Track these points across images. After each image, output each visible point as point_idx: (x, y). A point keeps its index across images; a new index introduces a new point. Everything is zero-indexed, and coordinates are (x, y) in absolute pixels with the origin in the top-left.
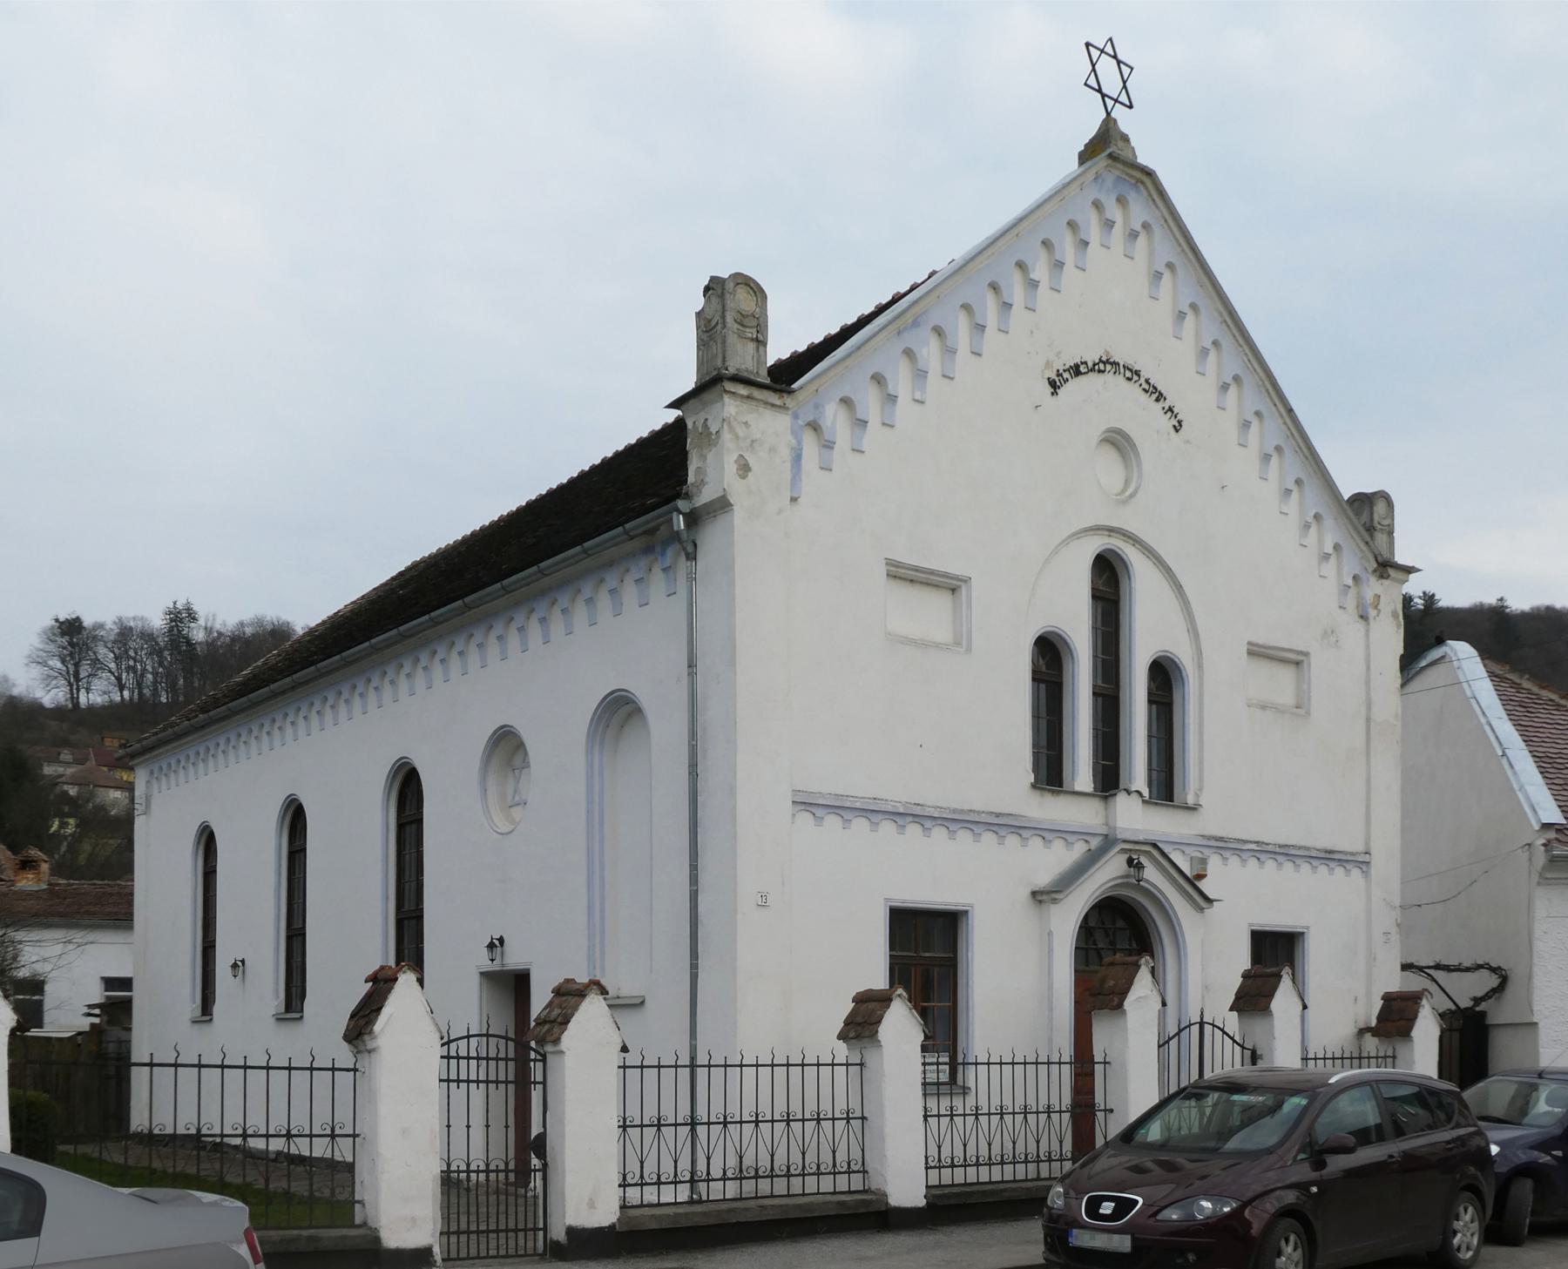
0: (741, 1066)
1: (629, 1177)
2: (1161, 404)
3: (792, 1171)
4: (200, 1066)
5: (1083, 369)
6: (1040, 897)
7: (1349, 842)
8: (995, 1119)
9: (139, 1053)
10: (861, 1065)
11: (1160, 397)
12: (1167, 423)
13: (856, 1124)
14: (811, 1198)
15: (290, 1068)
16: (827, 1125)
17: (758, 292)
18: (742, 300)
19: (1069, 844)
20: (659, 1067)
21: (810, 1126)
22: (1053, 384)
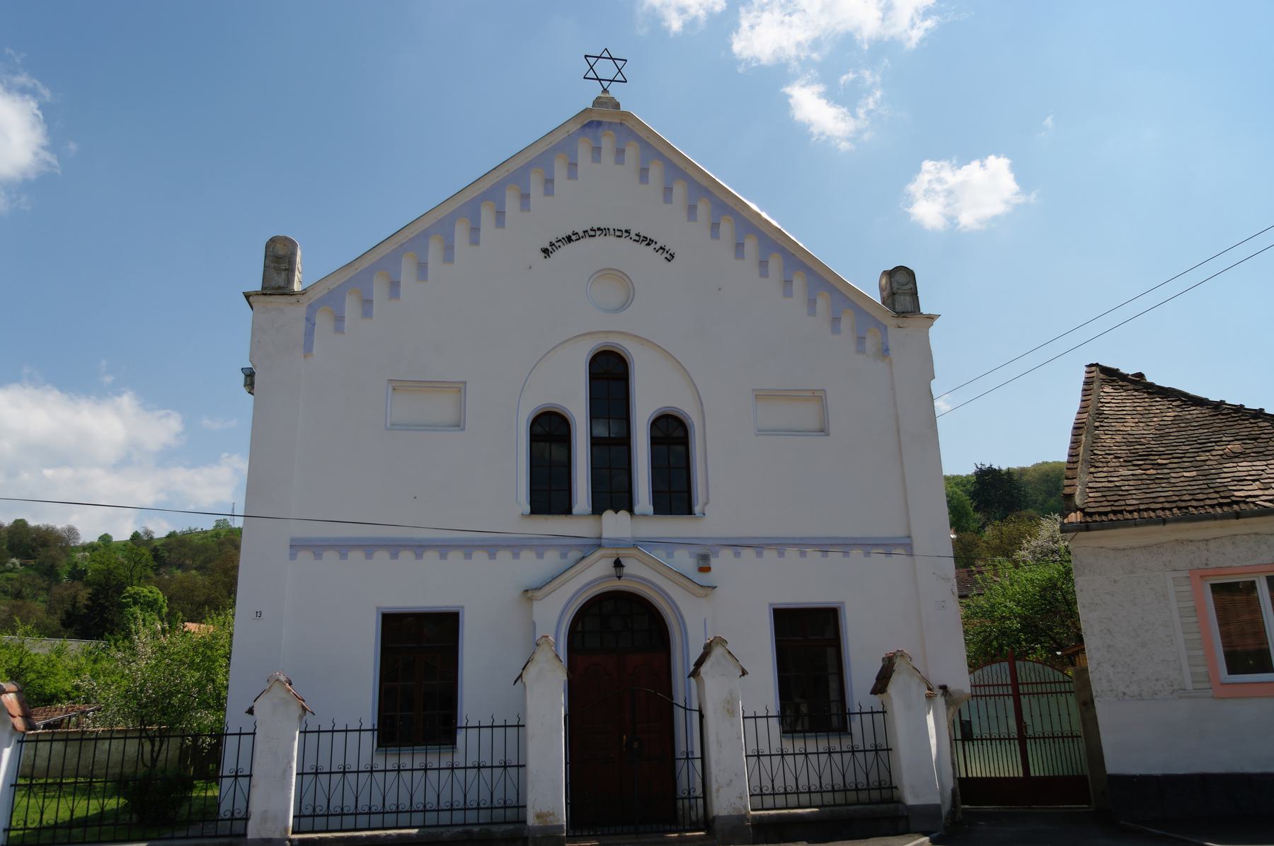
0: (360, 731)
1: (318, 810)
2: (653, 246)
3: (236, 815)
4: (319, 732)
5: (574, 238)
6: (529, 593)
7: (893, 530)
8: (871, 756)
9: (461, 721)
10: (884, 712)
11: (650, 242)
12: (660, 257)
13: (243, 782)
14: (431, 830)
15: (505, 726)
16: (813, 758)
17: (910, 274)
18: (281, 250)
19: (540, 556)
20: (240, 734)
21: (777, 760)
22: (545, 251)
